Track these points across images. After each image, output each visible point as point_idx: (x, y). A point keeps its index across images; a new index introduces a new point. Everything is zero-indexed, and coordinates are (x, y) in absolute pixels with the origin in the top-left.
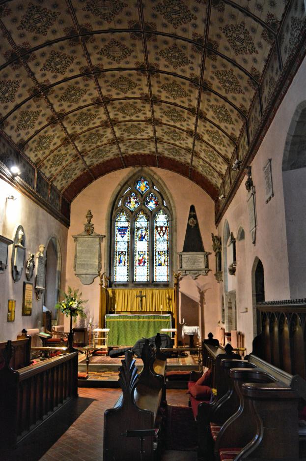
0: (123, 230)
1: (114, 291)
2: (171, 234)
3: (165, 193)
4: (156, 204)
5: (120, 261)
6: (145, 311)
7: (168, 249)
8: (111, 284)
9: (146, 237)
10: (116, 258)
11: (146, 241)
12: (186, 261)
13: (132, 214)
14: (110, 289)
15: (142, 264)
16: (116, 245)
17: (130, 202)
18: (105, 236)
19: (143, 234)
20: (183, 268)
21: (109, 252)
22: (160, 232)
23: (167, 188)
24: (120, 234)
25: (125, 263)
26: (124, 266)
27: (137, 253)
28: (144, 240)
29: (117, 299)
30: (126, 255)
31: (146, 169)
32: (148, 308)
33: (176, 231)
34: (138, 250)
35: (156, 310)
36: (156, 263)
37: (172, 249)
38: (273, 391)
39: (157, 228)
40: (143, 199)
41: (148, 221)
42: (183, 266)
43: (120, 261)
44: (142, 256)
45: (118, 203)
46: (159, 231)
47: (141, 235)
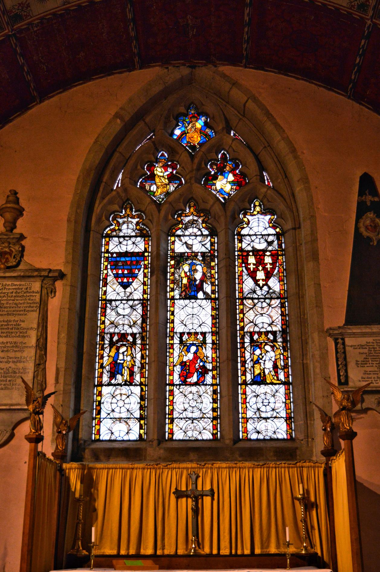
0: (126, 265)
1: (90, 476)
2: (294, 276)
3: (269, 145)
4: (238, 183)
5: (116, 368)
6: (211, 555)
7: (285, 323)
8: (80, 443)
9: (208, 288)
10: (102, 357)
11: (207, 297)
12: (360, 359)
13: (159, 211)
15: (194, 379)
16: (104, 314)
17: (152, 177)
18: (61, 276)
19: (198, 276)
20: (351, 384)
21: (75, 334)
22: (256, 270)
23: (277, 126)
24: (117, 276)
25: (132, 374)
26: (130, 383)
27: (176, 340)
28: (200, 295)
29: (100, 505)
30: (138, 347)
31: (205, 72)
32: (225, 543)
33: (315, 256)
34: (179, 328)
35: (258, 551)
36: (244, 373)
37: (302, 322)
38: (62, 502)
39: (244, 255)
40: (195, 168)
41: (213, 233)
42: (351, 374)
43: (116, 368)
44: (193, 349)
45: (113, 179)
46: (252, 267)
47: (191, 280)
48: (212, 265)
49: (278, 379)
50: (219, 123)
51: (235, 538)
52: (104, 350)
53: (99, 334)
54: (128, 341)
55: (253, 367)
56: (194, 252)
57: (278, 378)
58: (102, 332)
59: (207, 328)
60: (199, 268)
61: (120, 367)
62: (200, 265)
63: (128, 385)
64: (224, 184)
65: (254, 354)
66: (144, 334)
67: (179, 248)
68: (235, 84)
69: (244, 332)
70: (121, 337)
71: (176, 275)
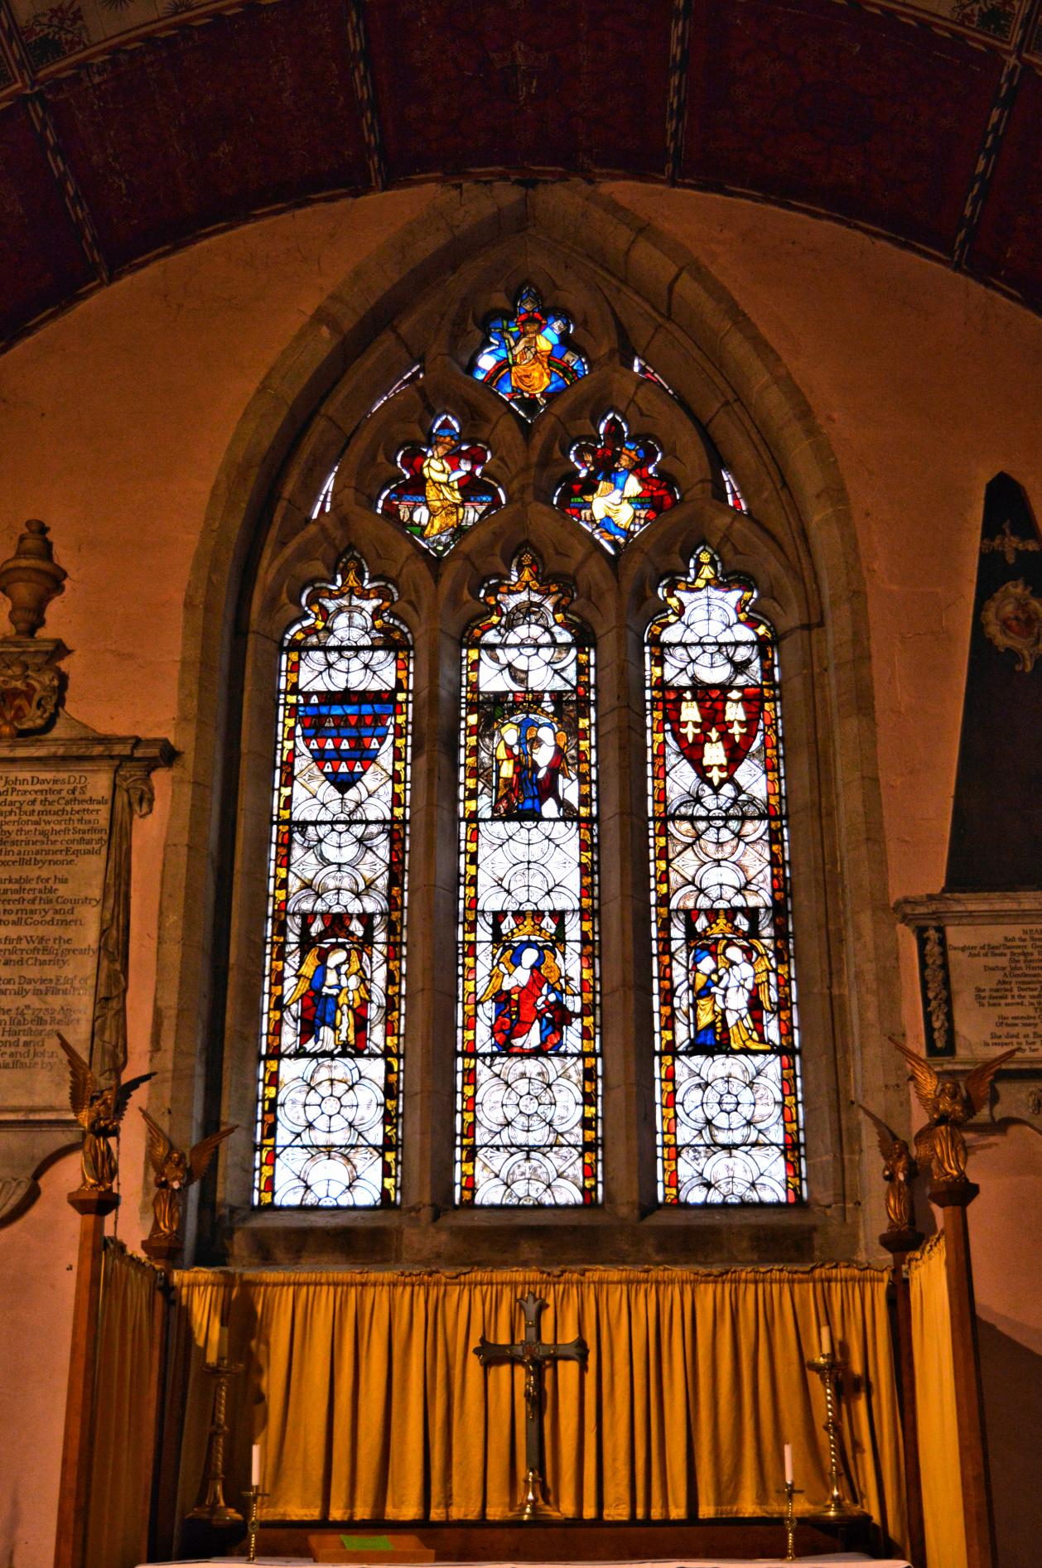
0: (346, 726)
1: (247, 1304)
2: (806, 757)
3: (738, 398)
4: (651, 503)
5: (317, 1010)
6: (578, 1521)
7: (780, 885)
8: (218, 1215)
9: (570, 790)
10: (279, 979)
11: (568, 814)
12: (988, 983)
13: (437, 578)
14: (205, 1274)
15: (533, 1038)
16: (285, 861)
17: (418, 486)
18: (169, 755)
19: (543, 756)
20: (962, 1052)
21: (205, 917)
22: (701, 740)
23: (760, 345)
24: (320, 757)
25: (361, 1024)
26: (355, 1049)
27: (484, 933)
28: (550, 808)
29: (273, 1383)
30: (379, 952)
31: (561, 198)
32: (616, 1489)
33: (863, 702)
34: (491, 900)
35: (706, 1511)
36: (669, 1024)
37: (829, 883)
39: (670, 699)
40: (536, 460)
41: (583, 639)
42: (962, 1027)
43: (317, 1010)
44: (530, 956)
45: (311, 491)
46: (690, 732)
47: (525, 767)
48: (581, 726)
49: (762, 1040)
50: (601, 338)
51: (645, 1474)
52: (285, 961)
53: (273, 917)
54: (352, 934)
55: (694, 1006)
56: (533, 692)
57: (761, 1035)
58: (279, 910)
59: (567, 900)
60: (546, 734)
61: (330, 1006)
62: (550, 726)
63: (352, 1056)
64: (615, 505)
65: (697, 971)
66: (395, 915)
67: (492, 679)
68: (643, 230)
69: (670, 911)
70: (332, 923)
71: (483, 754)
